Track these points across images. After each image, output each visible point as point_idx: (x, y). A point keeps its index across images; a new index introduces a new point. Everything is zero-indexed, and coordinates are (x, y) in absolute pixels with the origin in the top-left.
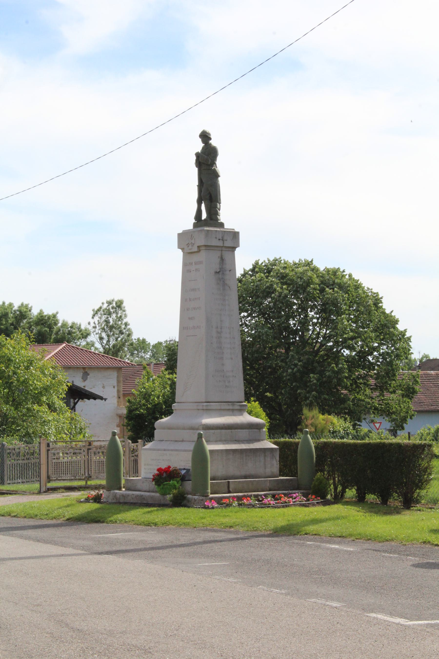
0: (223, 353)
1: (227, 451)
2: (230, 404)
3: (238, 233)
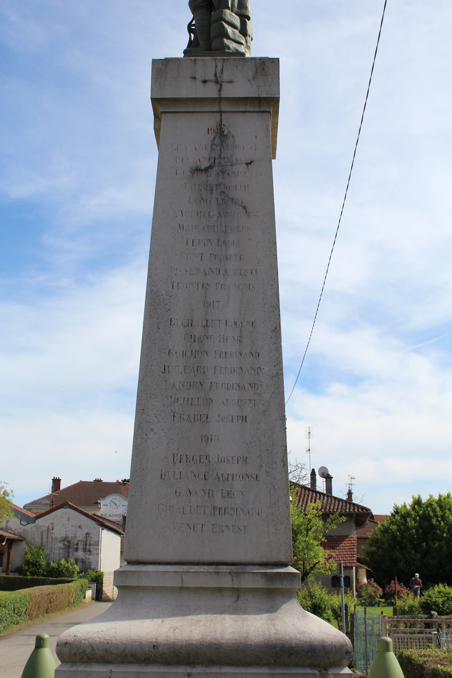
0: (209, 401)
3: (275, 62)
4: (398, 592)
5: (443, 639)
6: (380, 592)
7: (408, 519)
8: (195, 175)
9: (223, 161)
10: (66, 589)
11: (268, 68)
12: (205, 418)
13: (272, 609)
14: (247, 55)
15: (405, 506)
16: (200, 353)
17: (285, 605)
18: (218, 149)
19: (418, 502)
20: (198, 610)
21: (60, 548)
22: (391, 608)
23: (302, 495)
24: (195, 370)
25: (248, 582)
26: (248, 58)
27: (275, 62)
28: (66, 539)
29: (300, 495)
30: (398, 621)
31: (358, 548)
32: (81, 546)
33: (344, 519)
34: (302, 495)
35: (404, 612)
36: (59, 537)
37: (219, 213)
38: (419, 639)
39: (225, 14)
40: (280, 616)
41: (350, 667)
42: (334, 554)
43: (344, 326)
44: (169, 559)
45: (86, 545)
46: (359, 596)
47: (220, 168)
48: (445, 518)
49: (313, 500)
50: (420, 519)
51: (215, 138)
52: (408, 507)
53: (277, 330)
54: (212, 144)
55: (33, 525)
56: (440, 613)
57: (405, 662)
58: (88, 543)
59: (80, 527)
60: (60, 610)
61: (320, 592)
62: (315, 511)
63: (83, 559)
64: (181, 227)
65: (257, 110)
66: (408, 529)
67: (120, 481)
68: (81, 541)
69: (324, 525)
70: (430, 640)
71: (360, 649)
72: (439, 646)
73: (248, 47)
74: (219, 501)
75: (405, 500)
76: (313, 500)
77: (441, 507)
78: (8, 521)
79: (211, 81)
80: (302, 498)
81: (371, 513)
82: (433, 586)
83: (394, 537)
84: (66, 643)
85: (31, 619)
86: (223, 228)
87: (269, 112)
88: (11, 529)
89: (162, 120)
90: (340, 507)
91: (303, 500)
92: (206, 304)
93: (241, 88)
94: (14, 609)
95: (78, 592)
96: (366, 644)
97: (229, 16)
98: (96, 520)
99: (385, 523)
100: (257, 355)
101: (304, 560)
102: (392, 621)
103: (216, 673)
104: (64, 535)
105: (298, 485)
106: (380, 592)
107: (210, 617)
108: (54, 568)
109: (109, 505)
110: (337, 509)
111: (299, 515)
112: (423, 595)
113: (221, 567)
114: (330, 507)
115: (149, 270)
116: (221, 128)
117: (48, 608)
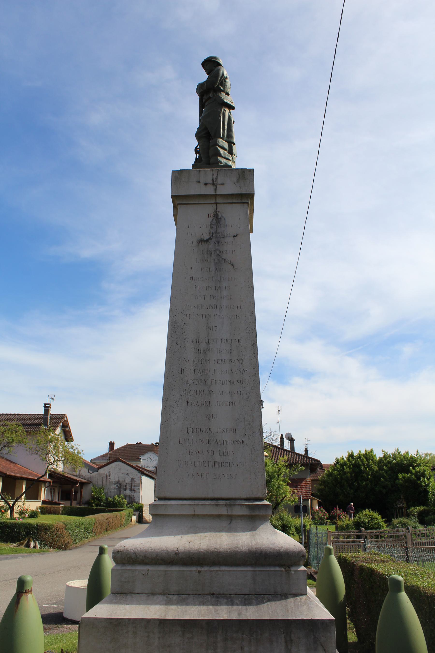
0: (210, 392)
1: (163, 623)
2: (222, 502)
3: (251, 171)
4: (339, 515)
5: (368, 546)
6: (327, 515)
7: (345, 467)
8: (200, 244)
9: (218, 235)
10: (119, 515)
11: (247, 175)
12: (208, 404)
13: (254, 529)
14: (233, 167)
15: (343, 458)
16: (204, 360)
17: (262, 526)
18: (215, 227)
19: (351, 455)
20: (204, 530)
21: (114, 488)
22: (334, 526)
23: (275, 452)
24: (201, 372)
25: (237, 511)
26: (234, 169)
27: (251, 171)
28: (118, 482)
29: (273, 452)
30: (338, 535)
31: (312, 486)
32: (128, 487)
33: (303, 468)
34: (275, 452)
35: (343, 529)
36: (114, 481)
37: (216, 269)
38: (352, 546)
39: (219, 142)
40: (258, 533)
41: (306, 566)
42: (296, 491)
43: (301, 339)
44: (186, 496)
45: (132, 486)
46: (313, 518)
47: (216, 239)
48: (369, 466)
49: (282, 455)
50: (353, 466)
51: (213, 220)
52: (345, 459)
53: (254, 345)
54: (211, 224)
55: (97, 473)
56: (366, 529)
57: (342, 562)
58: (133, 485)
59: (127, 474)
60: (115, 529)
61: (287, 517)
62: (283, 463)
63: (129, 496)
64: (191, 278)
65: (240, 202)
66: (345, 473)
67: (154, 444)
68: (128, 483)
69: (289, 472)
70: (359, 547)
71: (314, 553)
72: (365, 550)
73: (234, 162)
74: (218, 458)
75: (343, 455)
76: (282, 455)
77: (366, 458)
78: (80, 471)
79: (210, 184)
80: (274, 454)
81: (321, 463)
82: (362, 511)
83: (336, 479)
84: (119, 551)
85: (96, 535)
86: (219, 279)
87: (248, 203)
88: (82, 476)
89: (178, 209)
90: (300, 460)
91: (275, 455)
92: (208, 328)
93: (229, 187)
94: (85, 528)
95: (127, 517)
96: (318, 550)
97: (221, 143)
98: (138, 470)
99: (330, 470)
100: (242, 361)
101: (276, 495)
102: (334, 534)
103: (217, 571)
104: (117, 480)
105: (272, 445)
106: (327, 515)
107: (212, 534)
108: (110, 501)
109: (147, 460)
110: (298, 461)
111: (273, 466)
112: (355, 517)
113: (219, 501)
114: (293, 460)
115: (170, 306)
116: (217, 214)
117: (107, 528)
